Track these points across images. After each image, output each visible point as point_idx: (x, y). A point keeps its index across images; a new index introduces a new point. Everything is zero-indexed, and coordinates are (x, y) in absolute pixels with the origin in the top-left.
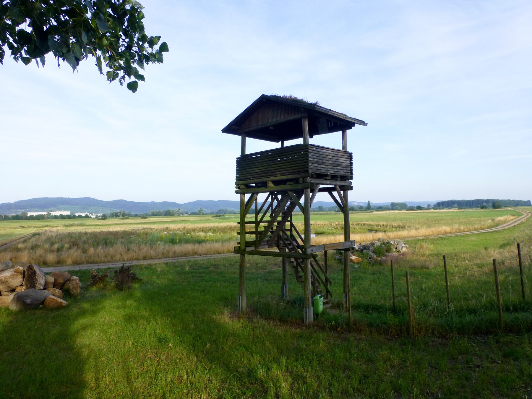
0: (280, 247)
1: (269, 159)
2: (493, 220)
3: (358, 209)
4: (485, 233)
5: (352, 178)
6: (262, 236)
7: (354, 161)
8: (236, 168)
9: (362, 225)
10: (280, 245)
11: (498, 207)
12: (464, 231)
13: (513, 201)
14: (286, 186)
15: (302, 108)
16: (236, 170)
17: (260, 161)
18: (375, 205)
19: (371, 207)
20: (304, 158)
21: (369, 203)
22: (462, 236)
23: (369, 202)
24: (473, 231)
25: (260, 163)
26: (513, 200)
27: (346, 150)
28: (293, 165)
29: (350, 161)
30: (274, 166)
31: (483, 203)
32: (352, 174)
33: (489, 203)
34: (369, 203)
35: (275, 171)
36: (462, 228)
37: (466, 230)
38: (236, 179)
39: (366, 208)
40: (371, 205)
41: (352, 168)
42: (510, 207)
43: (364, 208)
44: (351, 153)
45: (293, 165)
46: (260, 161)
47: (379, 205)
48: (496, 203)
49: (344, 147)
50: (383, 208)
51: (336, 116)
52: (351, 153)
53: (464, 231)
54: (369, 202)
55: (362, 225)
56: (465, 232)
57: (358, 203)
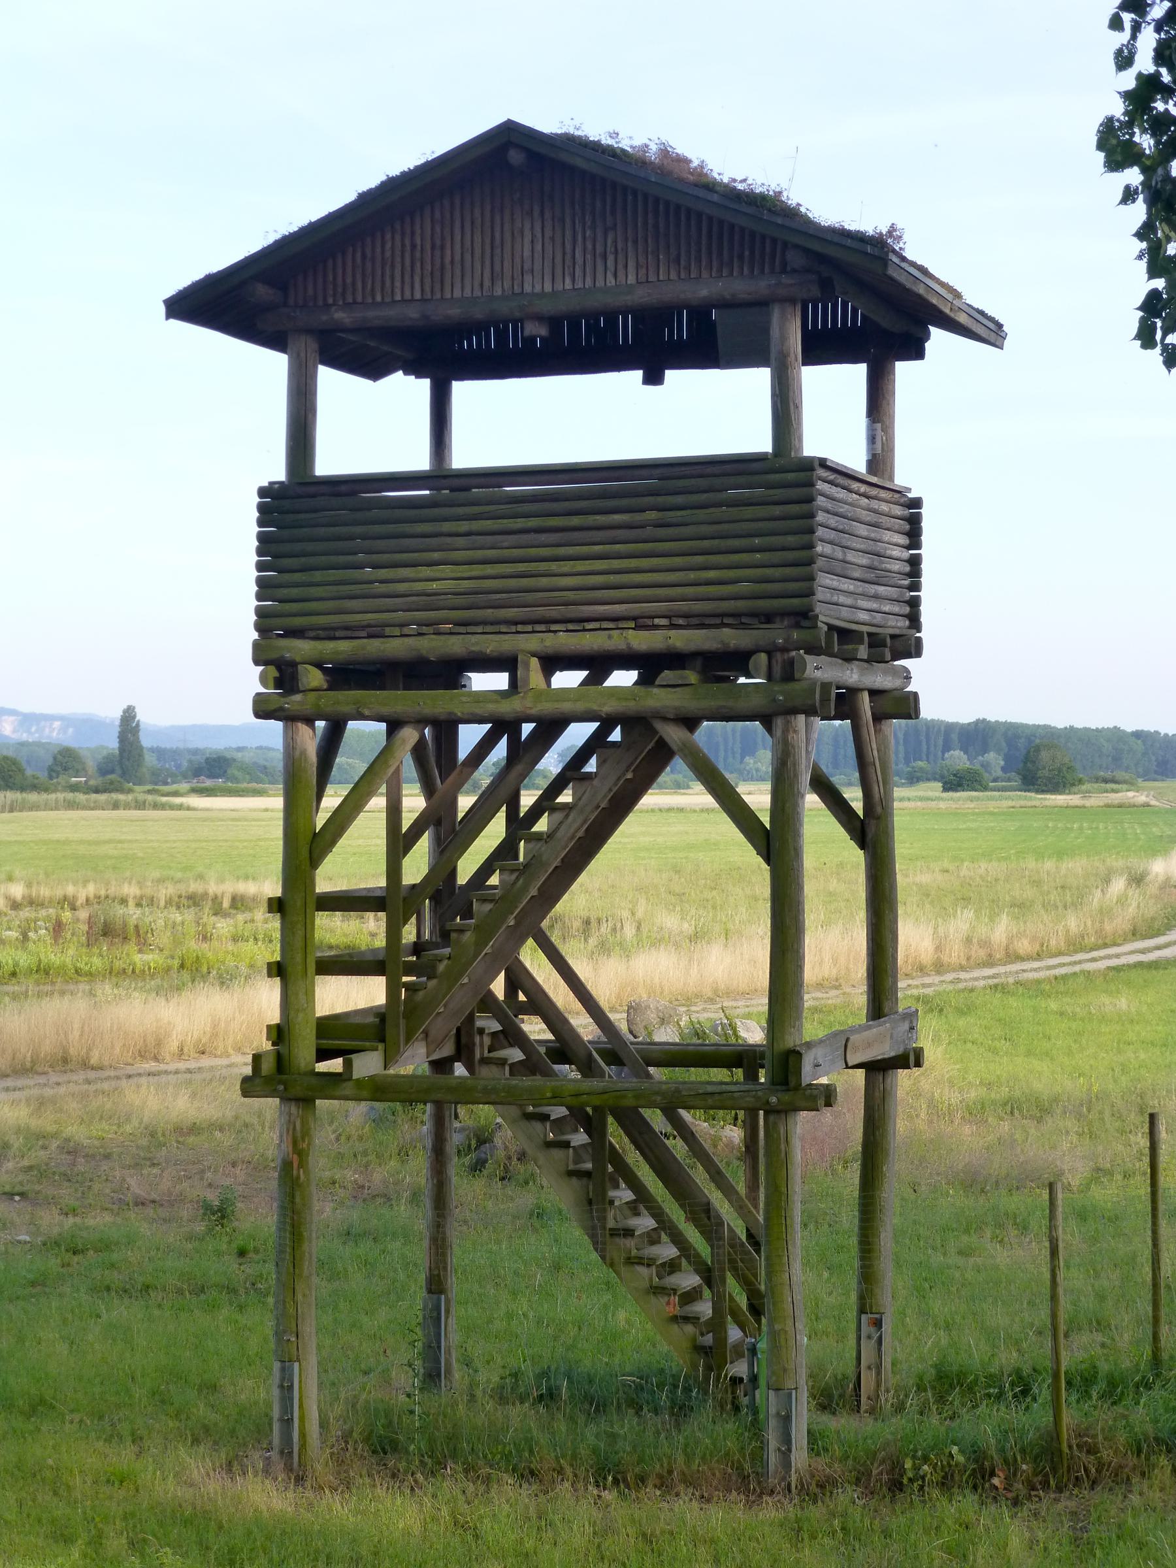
0: (478, 1056)
1: (533, 523)
2: (1138, 880)
3: (43, 776)
4: (1154, 965)
5: (914, 649)
6: (432, 983)
7: (928, 551)
8: (260, 552)
9: (226, 904)
10: (477, 1039)
11: (1057, 784)
12: (1013, 957)
13: (1139, 746)
14: (655, 690)
15: (797, 246)
16: (260, 567)
17: (464, 526)
18: (167, 745)
19: (150, 760)
20: (791, 540)
21: (129, 723)
22: (1035, 988)
23: (128, 719)
24: (1060, 954)
25: (461, 541)
26: (1138, 735)
27: (891, 479)
28: (711, 574)
29: (909, 548)
30: (567, 567)
31: (947, 747)
32: (914, 621)
33: (985, 750)
34: (129, 723)
35: (571, 595)
36: (1001, 931)
37: (1024, 946)
38: (259, 627)
39: (105, 768)
40: (146, 741)
41: (916, 586)
42: (1130, 784)
43: (91, 766)
44: (917, 503)
45: (711, 574)
46: (464, 526)
47: (200, 744)
48: (1044, 755)
49: (880, 460)
50: (233, 771)
51: (934, 301)
52: (917, 503)
53: (1013, 957)
54: (128, 719)
55: (226, 904)
56: (1019, 958)
57: (28, 719)
